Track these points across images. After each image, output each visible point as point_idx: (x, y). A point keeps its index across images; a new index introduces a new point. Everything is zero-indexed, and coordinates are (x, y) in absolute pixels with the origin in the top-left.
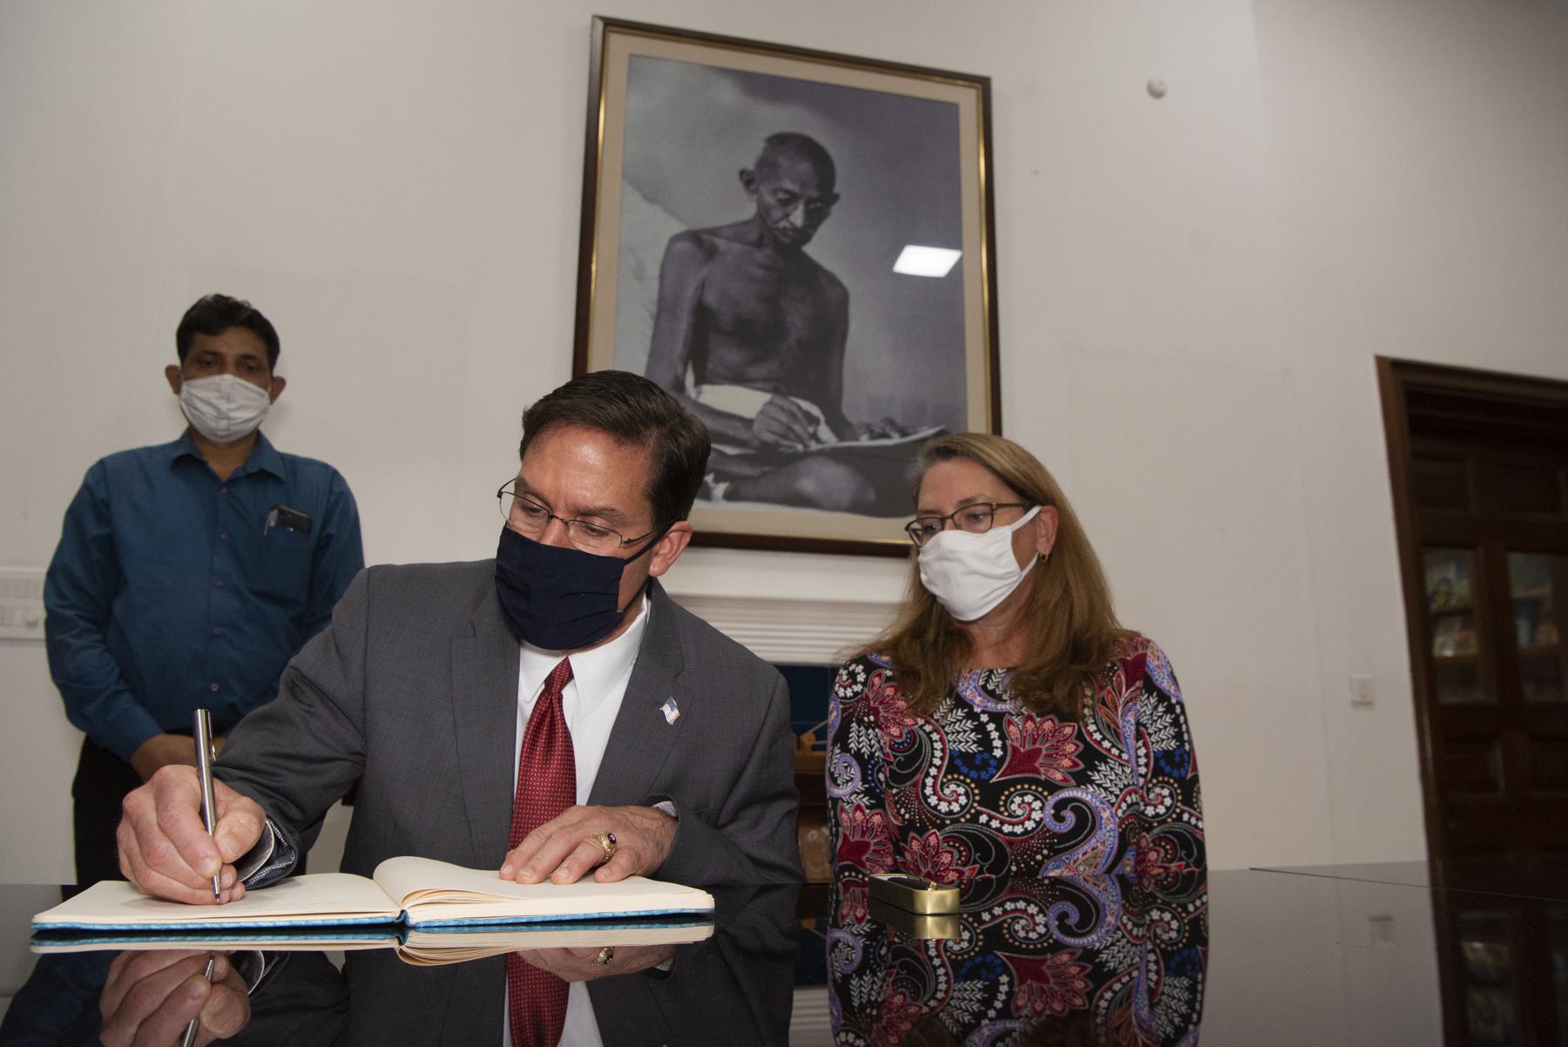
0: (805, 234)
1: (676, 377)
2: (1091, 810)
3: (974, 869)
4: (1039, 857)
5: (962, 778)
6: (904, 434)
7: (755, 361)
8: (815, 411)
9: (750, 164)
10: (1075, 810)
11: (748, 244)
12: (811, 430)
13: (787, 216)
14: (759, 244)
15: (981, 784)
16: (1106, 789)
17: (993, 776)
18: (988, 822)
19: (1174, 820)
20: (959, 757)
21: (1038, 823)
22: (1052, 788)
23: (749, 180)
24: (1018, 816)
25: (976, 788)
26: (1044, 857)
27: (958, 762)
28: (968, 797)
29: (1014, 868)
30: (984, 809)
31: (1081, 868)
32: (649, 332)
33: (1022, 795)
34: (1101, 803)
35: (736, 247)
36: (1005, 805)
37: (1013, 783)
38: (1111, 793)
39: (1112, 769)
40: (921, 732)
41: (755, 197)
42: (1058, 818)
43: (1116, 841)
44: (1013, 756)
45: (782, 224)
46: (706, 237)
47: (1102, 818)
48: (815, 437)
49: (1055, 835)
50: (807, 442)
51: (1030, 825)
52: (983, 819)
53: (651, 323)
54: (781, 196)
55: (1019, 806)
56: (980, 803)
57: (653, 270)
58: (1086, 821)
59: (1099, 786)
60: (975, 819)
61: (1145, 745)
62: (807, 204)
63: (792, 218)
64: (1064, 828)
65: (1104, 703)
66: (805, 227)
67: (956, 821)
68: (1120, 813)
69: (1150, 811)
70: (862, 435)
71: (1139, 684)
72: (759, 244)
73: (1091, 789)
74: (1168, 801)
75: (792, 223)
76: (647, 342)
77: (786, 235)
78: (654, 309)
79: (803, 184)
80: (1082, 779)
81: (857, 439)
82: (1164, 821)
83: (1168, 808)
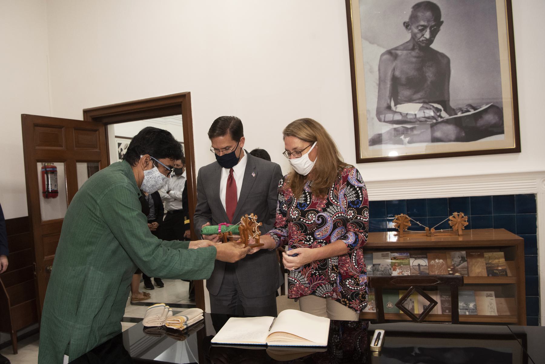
0: (430, 41)
1: (388, 104)
2: (326, 219)
3: (300, 232)
4: (314, 229)
5: (352, 208)
6: (475, 109)
7: (416, 92)
8: (439, 107)
9: (407, 19)
10: (322, 218)
11: (409, 50)
12: (438, 114)
13: (423, 35)
14: (413, 49)
15: (357, 209)
16: (330, 213)
17: (305, 209)
18: (303, 220)
19: (355, 219)
20: (350, 203)
21: (314, 221)
22: (318, 212)
23: (407, 25)
24: (310, 219)
25: (356, 210)
26: (315, 229)
27: (350, 204)
28: (354, 213)
29: (309, 232)
30: (302, 217)
31: (324, 232)
32: (377, 90)
33: (298, 214)
34: (328, 216)
35: (405, 52)
36: (307, 216)
37: (310, 210)
38: (331, 214)
39: (333, 207)
40: (293, 197)
41: (410, 31)
42: (318, 220)
43: (333, 226)
44: (312, 203)
45: (422, 39)
46: (393, 51)
47: (328, 220)
48: (440, 116)
49: (318, 224)
50: (437, 119)
51: (312, 221)
52: (302, 220)
53: (377, 87)
54: (420, 28)
55: (310, 216)
56: (357, 214)
57: (376, 68)
58: (324, 221)
59: (328, 212)
60: (300, 219)
61: (346, 200)
62: (430, 29)
63: (425, 36)
64: (319, 222)
65: (336, 189)
66: (430, 38)
67: (295, 220)
68: (333, 219)
69: (349, 217)
70: (459, 112)
71: (345, 183)
72: (413, 49)
73: (326, 213)
74: (353, 214)
75: (425, 38)
76: (377, 94)
77: (423, 43)
78: (378, 82)
79: (428, 21)
80: (324, 210)
81: (456, 114)
82: (352, 219)
83: (353, 216)
